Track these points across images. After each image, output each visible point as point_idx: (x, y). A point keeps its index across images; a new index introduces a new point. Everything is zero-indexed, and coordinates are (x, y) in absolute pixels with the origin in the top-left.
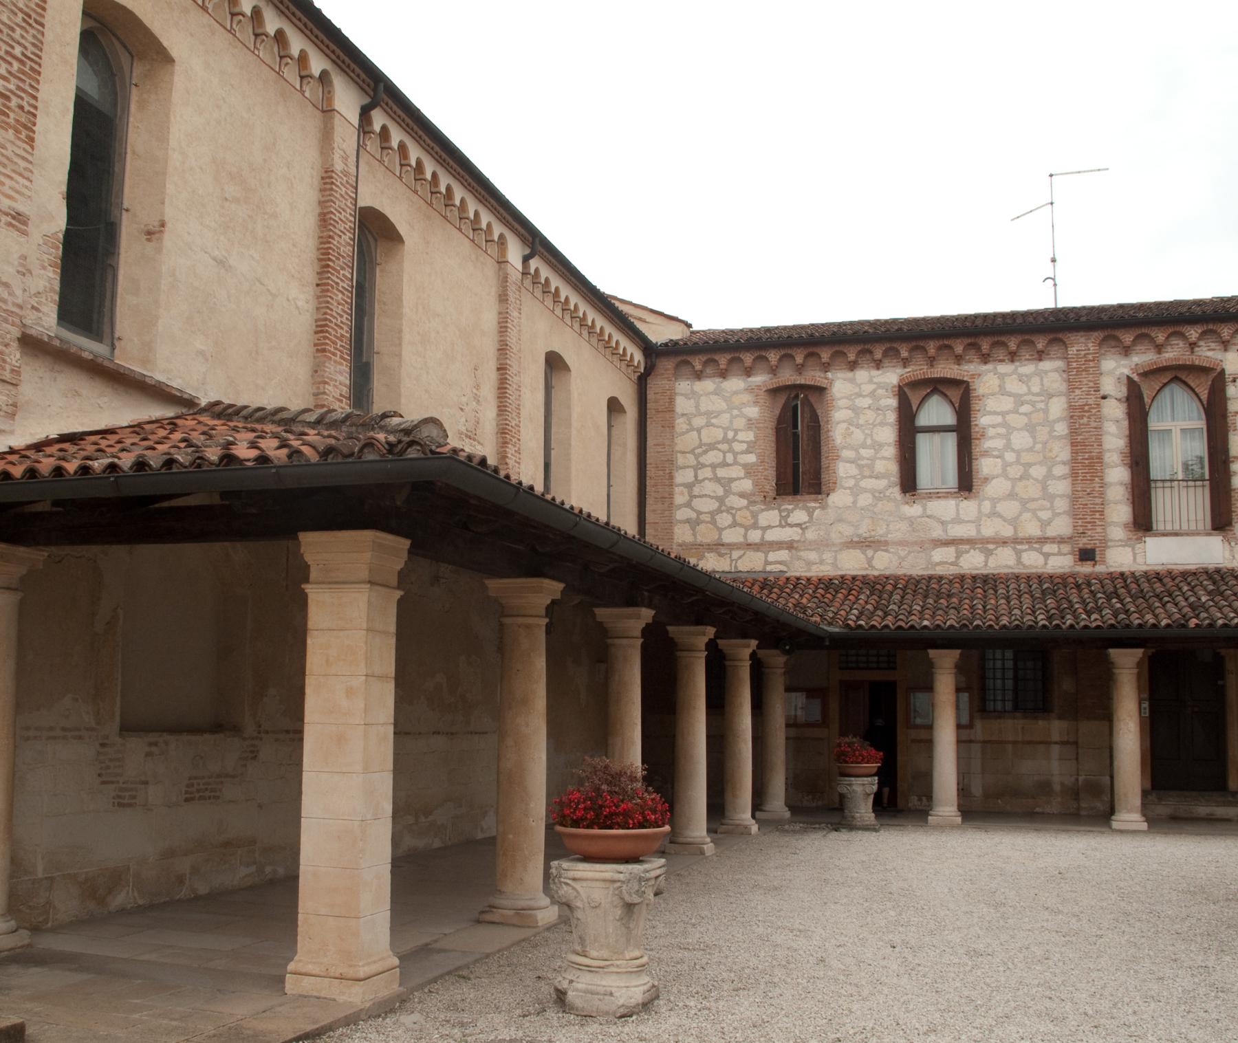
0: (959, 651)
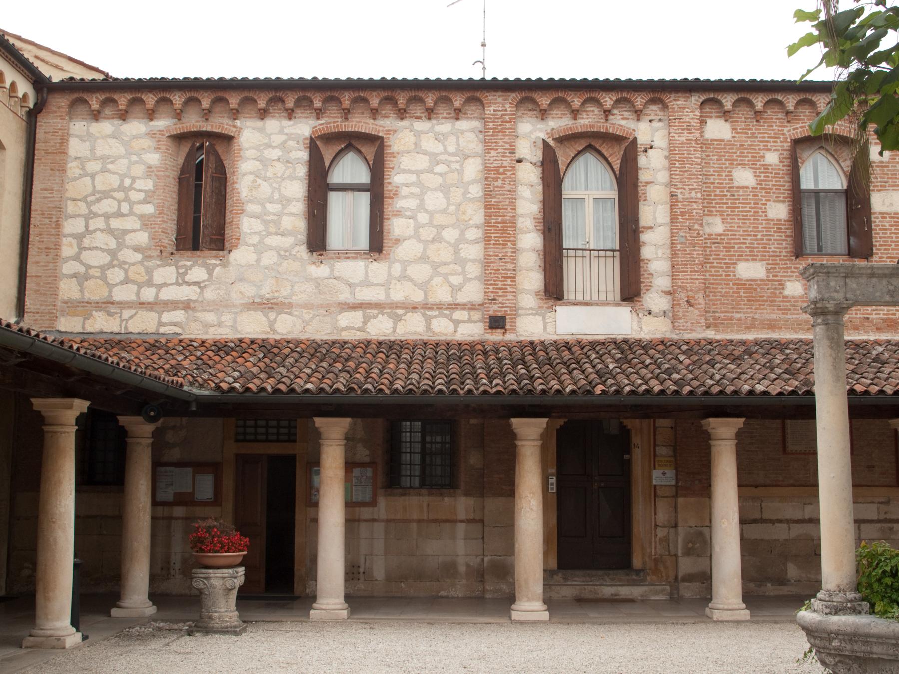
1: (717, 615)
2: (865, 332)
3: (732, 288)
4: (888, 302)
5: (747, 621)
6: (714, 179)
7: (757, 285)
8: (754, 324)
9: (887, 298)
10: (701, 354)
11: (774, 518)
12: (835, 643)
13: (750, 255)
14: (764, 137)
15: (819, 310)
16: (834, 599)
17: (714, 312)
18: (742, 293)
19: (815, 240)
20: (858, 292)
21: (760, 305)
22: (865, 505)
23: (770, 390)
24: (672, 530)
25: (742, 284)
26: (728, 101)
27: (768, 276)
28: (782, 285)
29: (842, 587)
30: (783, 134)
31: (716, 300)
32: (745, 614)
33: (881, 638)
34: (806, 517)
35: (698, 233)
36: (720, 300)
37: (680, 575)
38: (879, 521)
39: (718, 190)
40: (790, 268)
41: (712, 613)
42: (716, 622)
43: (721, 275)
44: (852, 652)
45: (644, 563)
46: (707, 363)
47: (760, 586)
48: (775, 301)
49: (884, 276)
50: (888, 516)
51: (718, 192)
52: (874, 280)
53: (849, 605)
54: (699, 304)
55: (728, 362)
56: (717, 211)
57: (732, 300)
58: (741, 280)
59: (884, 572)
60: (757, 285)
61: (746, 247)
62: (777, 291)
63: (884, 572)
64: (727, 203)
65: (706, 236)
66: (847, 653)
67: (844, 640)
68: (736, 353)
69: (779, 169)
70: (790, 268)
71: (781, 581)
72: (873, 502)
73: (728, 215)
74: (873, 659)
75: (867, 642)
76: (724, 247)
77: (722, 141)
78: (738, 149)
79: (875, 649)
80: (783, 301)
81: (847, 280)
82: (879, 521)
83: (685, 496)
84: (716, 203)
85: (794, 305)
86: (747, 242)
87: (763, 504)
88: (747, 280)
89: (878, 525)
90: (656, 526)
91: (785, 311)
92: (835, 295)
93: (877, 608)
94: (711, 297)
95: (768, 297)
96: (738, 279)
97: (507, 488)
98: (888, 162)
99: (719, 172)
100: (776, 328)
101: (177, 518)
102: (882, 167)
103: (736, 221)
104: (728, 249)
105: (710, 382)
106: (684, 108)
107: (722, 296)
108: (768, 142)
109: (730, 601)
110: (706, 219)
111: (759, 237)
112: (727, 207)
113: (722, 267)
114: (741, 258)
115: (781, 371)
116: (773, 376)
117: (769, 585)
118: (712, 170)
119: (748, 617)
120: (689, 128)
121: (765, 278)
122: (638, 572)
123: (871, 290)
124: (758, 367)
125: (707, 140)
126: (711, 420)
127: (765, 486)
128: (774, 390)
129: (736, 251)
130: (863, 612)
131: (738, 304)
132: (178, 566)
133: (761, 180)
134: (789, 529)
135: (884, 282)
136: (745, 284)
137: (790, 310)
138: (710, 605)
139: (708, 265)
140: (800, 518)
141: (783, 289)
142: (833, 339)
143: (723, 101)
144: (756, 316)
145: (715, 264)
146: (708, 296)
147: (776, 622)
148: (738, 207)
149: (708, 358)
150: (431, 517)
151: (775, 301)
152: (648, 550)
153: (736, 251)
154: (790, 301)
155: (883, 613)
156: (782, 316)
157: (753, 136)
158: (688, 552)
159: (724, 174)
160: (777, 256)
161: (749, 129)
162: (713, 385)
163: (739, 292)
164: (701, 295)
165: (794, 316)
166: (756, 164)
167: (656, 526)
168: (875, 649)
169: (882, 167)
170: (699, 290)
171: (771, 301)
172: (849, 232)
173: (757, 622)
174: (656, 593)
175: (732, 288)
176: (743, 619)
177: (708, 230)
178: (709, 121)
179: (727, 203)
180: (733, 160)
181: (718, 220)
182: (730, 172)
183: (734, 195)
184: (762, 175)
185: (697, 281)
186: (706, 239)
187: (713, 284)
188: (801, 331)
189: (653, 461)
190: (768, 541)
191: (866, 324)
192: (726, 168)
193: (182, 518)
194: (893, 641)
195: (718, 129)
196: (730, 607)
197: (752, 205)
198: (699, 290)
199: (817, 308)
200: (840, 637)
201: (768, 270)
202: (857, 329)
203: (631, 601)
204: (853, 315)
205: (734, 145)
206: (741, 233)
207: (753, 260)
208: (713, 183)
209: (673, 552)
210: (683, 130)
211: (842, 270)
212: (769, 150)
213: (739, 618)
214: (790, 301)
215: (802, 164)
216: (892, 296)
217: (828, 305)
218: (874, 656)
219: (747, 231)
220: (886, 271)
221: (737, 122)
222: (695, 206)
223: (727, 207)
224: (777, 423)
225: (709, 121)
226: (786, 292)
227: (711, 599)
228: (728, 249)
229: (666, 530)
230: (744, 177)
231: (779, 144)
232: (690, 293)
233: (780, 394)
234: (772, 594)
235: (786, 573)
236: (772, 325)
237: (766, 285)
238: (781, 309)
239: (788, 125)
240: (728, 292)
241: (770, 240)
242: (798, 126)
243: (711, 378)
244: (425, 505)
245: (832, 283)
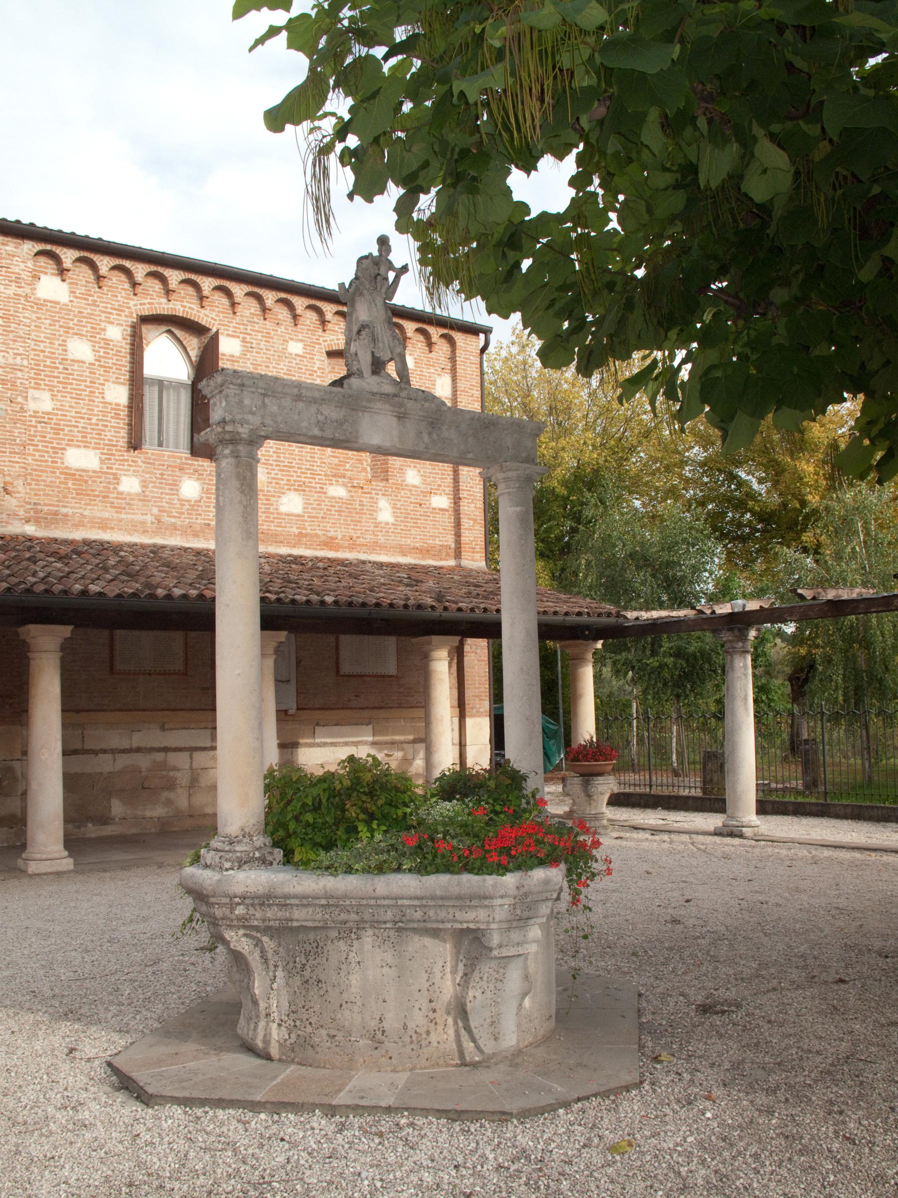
1: (33, 867)
2: (205, 539)
3: (59, 478)
4: (315, 437)
5: (70, 872)
6: (45, 347)
7: (87, 476)
8: (83, 522)
9: (316, 432)
10: (18, 551)
11: (98, 748)
12: (240, 910)
13: (82, 442)
14: (106, 308)
15: (227, 437)
16: (238, 848)
17: (35, 504)
18: (70, 485)
19: (156, 434)
20: (280, 419)
21: (91, 500)
22: (198, 731)
23: (106, 591)
25: (71, 474)
26: (68, 256)
27: (101, 468)
28: (116, 478)
29: (247, 830)
30: (129, 308)
31: (39, 490)
32: (68, 864)
33: (306, 900)
34: (134, 746)
35: (22, 408)
36: (44, 490)
39: (48, 360)
40: (127, 460)
41: (27, 864)
43: (47, 461)
44: (264, 920)
46: (29, 559)
47: (79, 827)
48: (108, 497)
49: (314, 401)
51: (48, 363)
52: (300, 405)
53: (257, 855)
54: (18, 492)
55: (53, 560)
56: (45, 385)
57: (59, 492)
58: (70, 469)
59: (304, 805)
60: (87, 476)
61: (78, 432)
62: (112, 486)
63: (304, 805)
64: (58, 377)
65: (32, 413)
66: (256, 923)
67: (253, 905)
68: (62, 552)
69: (121, 347)
70: (127, 460)
71: (104, 820)
72: (206, 728)
73: (58, 391)
74: (292, 929)
75: (286, 905)
76: (52, 428)
77: (58, 303)
78: (75, 316)
79: (297, 914)
80: (117, 498)
81: (267, 400)
84: (45, 376)
85: (129, 504)
86: (80, 425)
87: (86, 732)
88: (78, 470)
91: (119, 509)
92: (250, 417)
93: (297, 857)
94: (33, 486)
95: (101, 491)
96: (67, 468)
98: (240, 358)
99: (51, 339)
100: (107, 528)
102: (233, 361)
103: (68, 399)
104: (57, 430)
105: (33, 580)
106: (14, 256)
107: (47, 486)
108: (110, 313)
109: (49, 849)
110: (31, 392)
111: (94, 421)
112: (58, 382)
113: (48, 452)
114: (71, 443)
115: (117, 572)
116: (109, 577)
117: (90, 825)
118: (42, 335)
119: (72, 867)
120: (18, 280)
121: (98, 469)
123: (296, 417)
124: (89, 567)
125: (39, 299)
127: (89, 711)
128: (112, 591)
129: (66, 435)
130: (275, 863)
131: (65, 497)
133: (100, 356)
134: (115, 760)
135: (313, 409)
136: (74, 475)
137: (124, 508)
138: (24, 855)
139: (31, 448)
140: (128, 747)
141: (118, 484)
142: (245, 478)
143: (62, 257)
144: (86, 513)
145: (40, 448)
146: (30, 484)
147: (105, 871)
148: (71, 384)
149: (28, 555)
151: (108, 497)
153: (66, 435)
154: (125, 499)
155: (305, 864)
156: (116, 515)
157: (94, 304)
159: (57, 343)
160: (113, 445)
161: (90, 295)
162: (36, 583)
163: (67, 484)
164: (20, 482)
165: (129, 516)
166: (94, 336)
168: (297, 914)
169: (233, 361)
170: (19, 476)
171: (104, 497)
173: (82, 872)
175: (59, 478)
176: (65, 869)
177: (32, 406)
178: (43, 277)
179: (58, 377)
180: (69, 328)
181: (46, 395)
182: (65, 341)
183: (67, 369)
184: (102, 350)
185: (17, 465)
186: (30, 416)
187: (36, 470)
188: (136, 534)
190: (90, 774)
191: (207, 531)
192: (60, 336)
194: (324, 902)
195: (51, 287)
196: (49, 857)
197: (88, 384)
198: (19, 476)
199: (225, 432)
200: (247, 901)
201: (102, 462)
202: (197, 536)
204: (194, 521)
205: (70, 310)
206: (73, 414)
207: (85, 447)
208: (43, 351)
210: (11, 281)
211: (261, 384)
212: (112, 323)
213: (60, 869)
214: (125, 499)
215: (147, 345)
216: (322, 430)
217: (241, 430)
218: (295, 924)
219: (80, 413)
220: (317, 395)
221: (77, 284)
222: (19, 374)
223: (58, 382)
225: (43, 277)
226: (121, 488)
227: (24, 847)
228: (57, 430)
230: (80, 350)
231: (124, 318)
232: (8, 479)
233: (119, 596)
234: (93, 835)
235: (110, 811)
236: (103, 525)
237: (99, 477)
238: (115, 507)
239: (135, 298)
240: (55, 482)
241: (106, 426)
242: (146, 301)
243: (34, 574)
245: (247, 402)
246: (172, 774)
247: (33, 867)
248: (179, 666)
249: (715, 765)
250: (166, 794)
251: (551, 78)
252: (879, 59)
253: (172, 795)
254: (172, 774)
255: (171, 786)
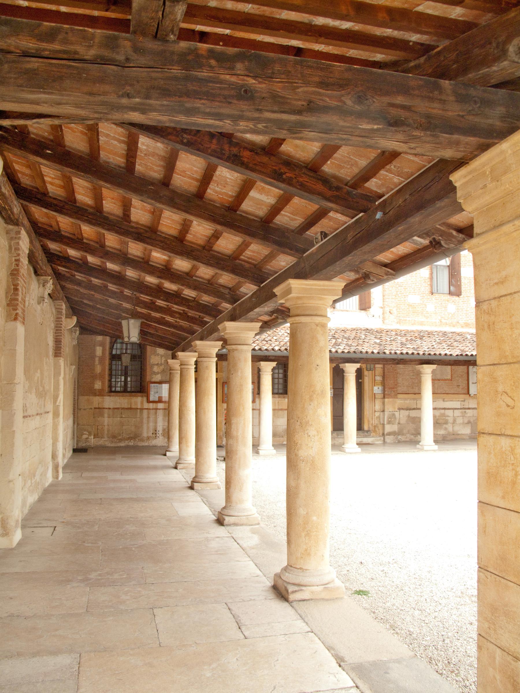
0: (276, 363)
24: (382, 413)
37: (386, 433)
38: (461, 409)
42: (426, 451)
45: (369, 428)
50: (465, 407)
82: (461, 409)
83: (388, 398)
89: (461, 410)
90: (375, 411)
97: (418, 394)
101: (159, 409)
122: (367, 431)
126: (347, 364)
132: (160, 432)
150: (280, 408)
152: (371, 422)
158: (389, 423)
167: (375, 411)
172: (450, 284)
173: (441, 450)
174: (378, 441)
189: (374, 383)
193: (163, 409)
203: (368, 444)
209: (382, 422)
224: (465, 367)
229: (379, 413)
232: (391, 308)
236: (422, 324)
244: (277, 402)
246: (447, 418)
247: (426, 448)
248: (449, 377)
249: (416, 423)
250: (445, 426)
251: (503, 72)
252: (49, 152)
253: (446, 426)
254: (447, 418)
255: (446, 423)
